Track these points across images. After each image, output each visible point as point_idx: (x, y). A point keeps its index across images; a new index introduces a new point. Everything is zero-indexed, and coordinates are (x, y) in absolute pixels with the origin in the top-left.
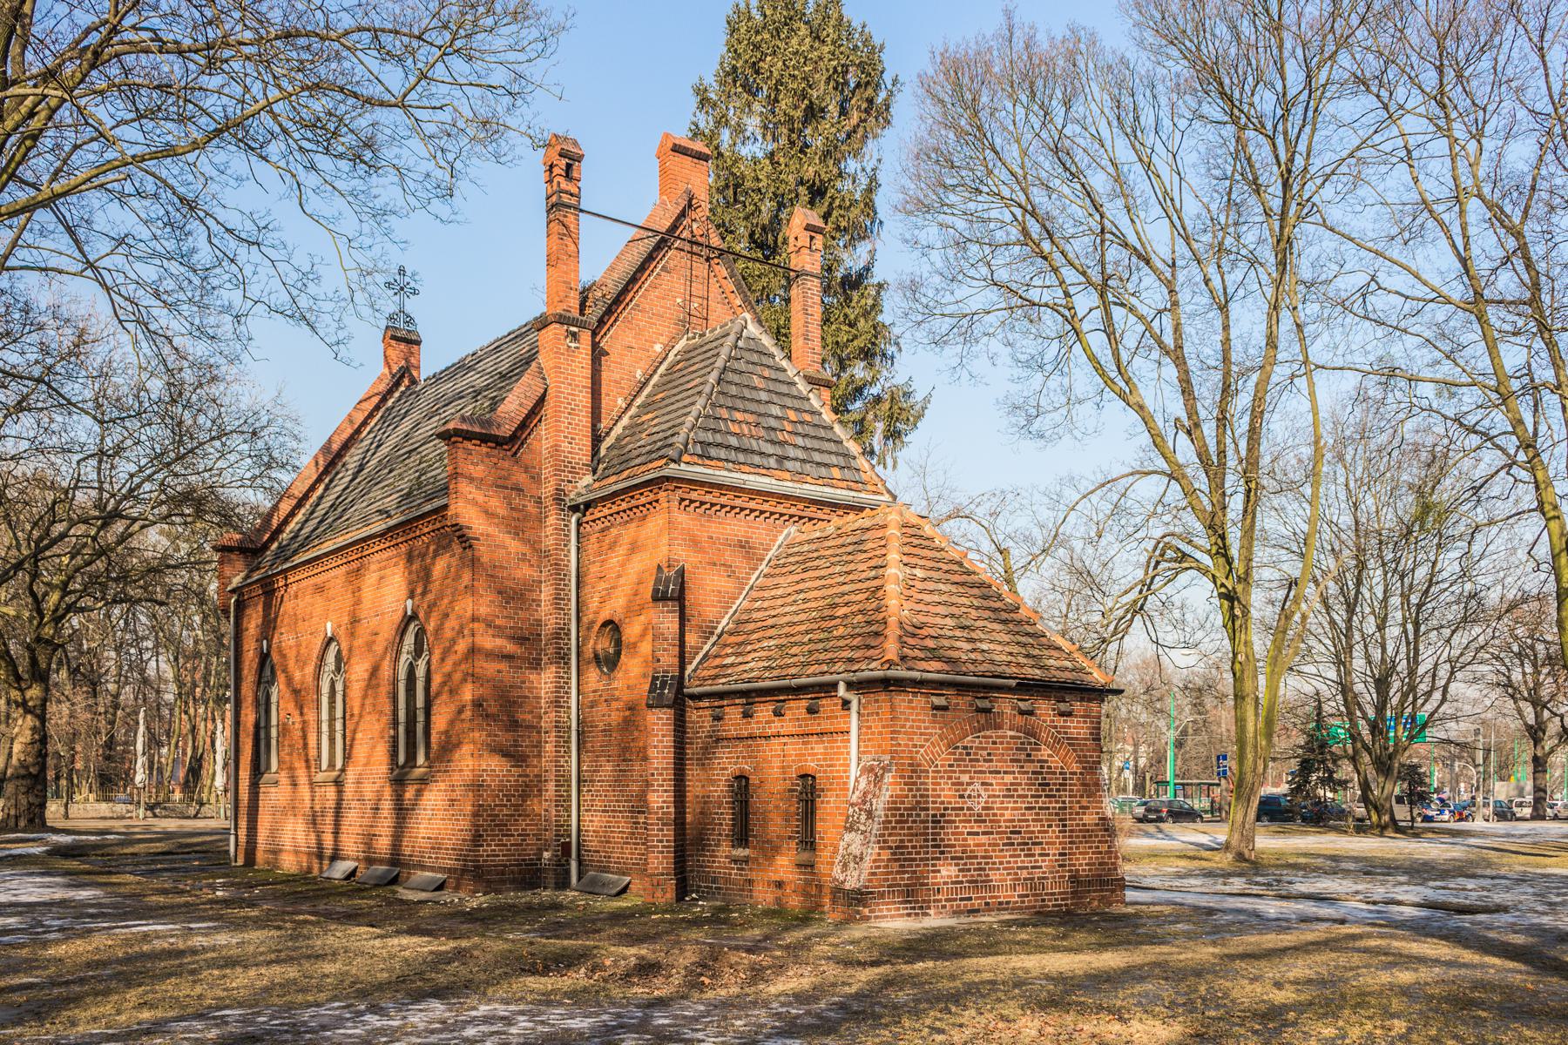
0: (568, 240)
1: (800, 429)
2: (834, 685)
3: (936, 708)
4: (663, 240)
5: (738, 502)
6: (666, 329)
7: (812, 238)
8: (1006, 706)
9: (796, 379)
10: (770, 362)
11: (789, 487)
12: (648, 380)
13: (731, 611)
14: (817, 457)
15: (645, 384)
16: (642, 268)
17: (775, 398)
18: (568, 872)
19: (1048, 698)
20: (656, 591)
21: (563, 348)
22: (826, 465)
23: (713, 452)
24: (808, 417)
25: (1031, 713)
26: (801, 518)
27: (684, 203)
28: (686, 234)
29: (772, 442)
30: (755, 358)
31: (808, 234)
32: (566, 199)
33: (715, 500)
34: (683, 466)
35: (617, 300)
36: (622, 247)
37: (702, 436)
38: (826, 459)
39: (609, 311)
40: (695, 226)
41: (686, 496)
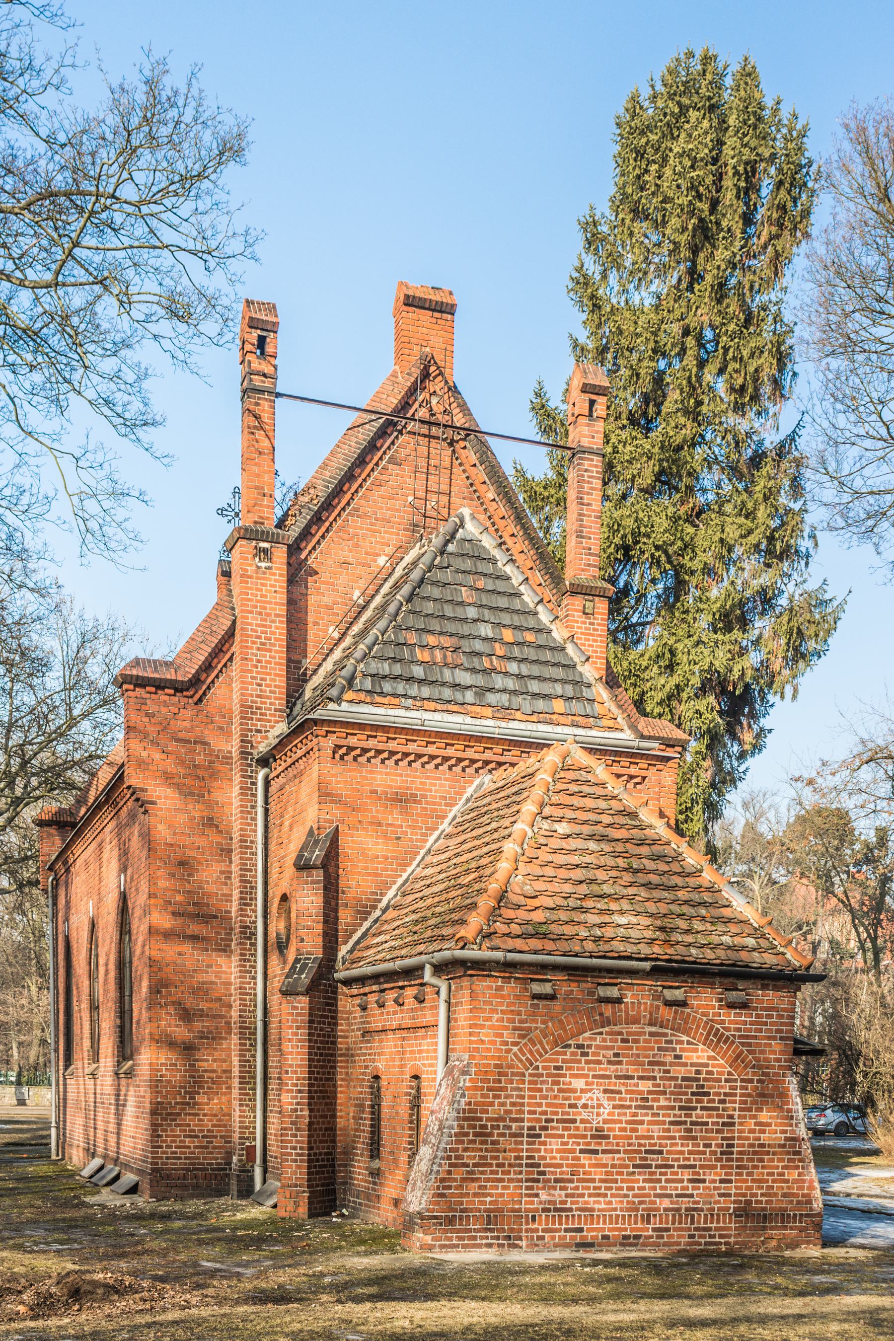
0: (260, 434)
1: (516, 652)
2: (421, 968)
3: (535, 997)
4: (390, 423)
5: (412, 747)
6: (394, 536)
7: (592, 403)
8: (637, 996)
9: (522, 588)
10: (489, 569)
11: (490, 726)
12: (368, 603)
13: (400, 881)
14: (534, 686)
15: (364, 607)
16: (361, 461)
17: (487, 614)
18: (252, 1179)
19: (712, 985)
20: (300, 857)
21: (251, 570)
22: (545, 697)
23: (387, 687)
24: (530, 637)
25: (684, 1004)
26: (500, 764)
27: (416, 372)
28: (423, 413)
29: (473, 670)
30: (468, 564)
31: (587, 397)
32: (258, 381)
33: (381, 747)
34: (345, 706)
35: (328, 505)
37: (375, 666)
38: (546, 688)
39: (317, 519)
40: (434, 400)
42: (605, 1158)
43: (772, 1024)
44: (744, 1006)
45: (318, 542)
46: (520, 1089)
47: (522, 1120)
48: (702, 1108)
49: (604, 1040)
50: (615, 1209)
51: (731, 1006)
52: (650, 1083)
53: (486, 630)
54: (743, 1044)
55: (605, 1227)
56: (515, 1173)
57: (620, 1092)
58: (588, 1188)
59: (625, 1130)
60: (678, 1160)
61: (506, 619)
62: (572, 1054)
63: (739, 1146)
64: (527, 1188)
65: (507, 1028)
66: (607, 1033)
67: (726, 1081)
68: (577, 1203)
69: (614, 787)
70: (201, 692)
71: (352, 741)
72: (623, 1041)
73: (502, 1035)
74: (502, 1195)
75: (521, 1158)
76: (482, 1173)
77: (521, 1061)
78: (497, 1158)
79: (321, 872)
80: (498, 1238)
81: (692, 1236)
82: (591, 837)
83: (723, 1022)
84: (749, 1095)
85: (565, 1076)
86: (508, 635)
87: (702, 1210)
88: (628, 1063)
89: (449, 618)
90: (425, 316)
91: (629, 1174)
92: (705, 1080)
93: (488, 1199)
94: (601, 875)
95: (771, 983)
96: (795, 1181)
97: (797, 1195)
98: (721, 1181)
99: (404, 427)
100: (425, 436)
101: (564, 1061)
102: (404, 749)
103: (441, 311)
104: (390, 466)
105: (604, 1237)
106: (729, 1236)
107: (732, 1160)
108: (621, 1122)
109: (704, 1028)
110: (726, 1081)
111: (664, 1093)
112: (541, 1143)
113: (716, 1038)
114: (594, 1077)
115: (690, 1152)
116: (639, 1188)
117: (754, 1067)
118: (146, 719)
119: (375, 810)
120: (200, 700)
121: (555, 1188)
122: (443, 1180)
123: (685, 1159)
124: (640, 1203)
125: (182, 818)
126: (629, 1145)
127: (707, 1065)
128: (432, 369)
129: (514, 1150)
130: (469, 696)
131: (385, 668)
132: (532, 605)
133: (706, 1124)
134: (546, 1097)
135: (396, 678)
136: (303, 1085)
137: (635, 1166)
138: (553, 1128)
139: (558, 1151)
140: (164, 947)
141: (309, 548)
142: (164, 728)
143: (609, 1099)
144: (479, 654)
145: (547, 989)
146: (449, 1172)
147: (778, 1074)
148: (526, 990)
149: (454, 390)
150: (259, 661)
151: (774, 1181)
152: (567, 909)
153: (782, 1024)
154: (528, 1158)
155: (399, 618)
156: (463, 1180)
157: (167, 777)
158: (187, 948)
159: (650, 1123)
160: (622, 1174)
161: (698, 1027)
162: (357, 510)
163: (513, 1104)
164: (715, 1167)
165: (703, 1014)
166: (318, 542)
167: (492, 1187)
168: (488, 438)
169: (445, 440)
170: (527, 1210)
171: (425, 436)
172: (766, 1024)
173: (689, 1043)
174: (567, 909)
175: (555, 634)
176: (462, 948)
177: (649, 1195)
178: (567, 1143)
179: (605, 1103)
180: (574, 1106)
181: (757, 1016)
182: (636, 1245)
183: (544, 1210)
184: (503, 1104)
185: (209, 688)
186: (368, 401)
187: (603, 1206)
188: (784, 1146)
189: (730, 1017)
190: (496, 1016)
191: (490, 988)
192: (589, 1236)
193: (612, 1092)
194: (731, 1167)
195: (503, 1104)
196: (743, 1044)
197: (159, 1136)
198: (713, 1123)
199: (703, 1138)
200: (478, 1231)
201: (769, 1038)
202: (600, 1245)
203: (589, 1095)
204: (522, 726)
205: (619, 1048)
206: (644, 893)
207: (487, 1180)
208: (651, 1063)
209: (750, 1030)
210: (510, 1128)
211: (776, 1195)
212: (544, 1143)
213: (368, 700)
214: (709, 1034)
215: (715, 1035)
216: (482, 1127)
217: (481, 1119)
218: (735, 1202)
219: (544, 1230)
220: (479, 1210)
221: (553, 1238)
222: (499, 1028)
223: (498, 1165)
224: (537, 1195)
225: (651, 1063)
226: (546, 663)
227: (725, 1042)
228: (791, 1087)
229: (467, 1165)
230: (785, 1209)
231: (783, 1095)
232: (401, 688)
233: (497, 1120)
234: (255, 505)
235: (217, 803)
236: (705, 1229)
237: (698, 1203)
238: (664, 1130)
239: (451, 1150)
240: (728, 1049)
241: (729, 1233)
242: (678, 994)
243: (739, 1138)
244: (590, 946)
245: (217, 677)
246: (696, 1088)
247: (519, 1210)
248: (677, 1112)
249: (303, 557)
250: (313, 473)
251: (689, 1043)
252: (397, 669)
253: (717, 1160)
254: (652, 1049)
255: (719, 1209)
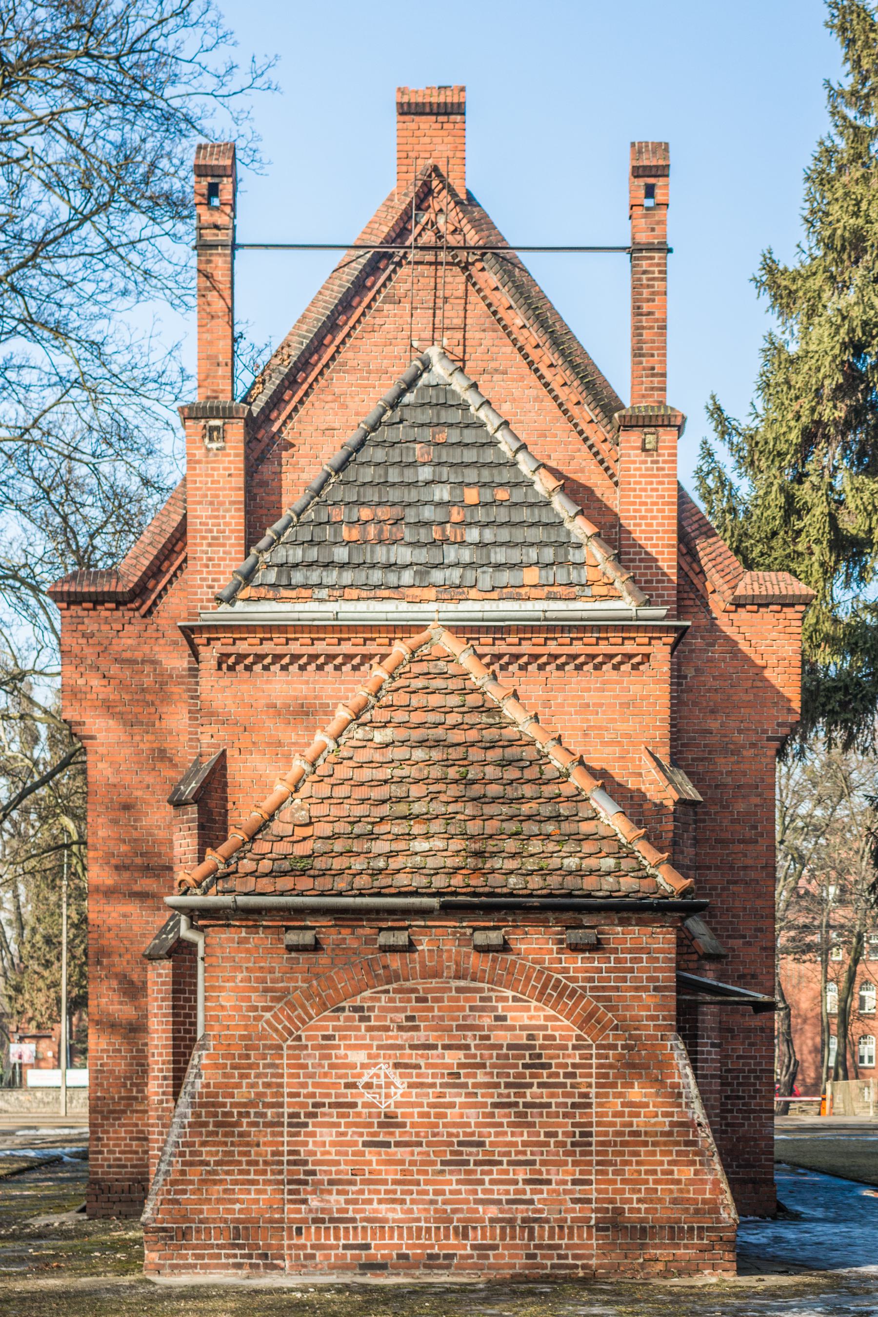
0: (212, 296)
3: (290, 948)
8: (438, 942)
9: (499, 435)
14: (499, 555)
16: (345, 305)
19: (545, 923)
23: (298, 577)
28: (429, 237)
29: (416, 544)
30: (429, 415)
32: (210, 236)
33: (279, 650)
35: (303, 363)
36: (329, 274)
38: (515, 555)
40: (441, 220)
41: (230, 649)
42: (400, 1153)
43: (640, 970)
44: (597, 947)
45: (295, 409)
46: (276, 1066)
47: (281, 1105)
48: (541, 1085)
49: (392, 1000)
50: (418, 1220)
51: (575, 948)
52: (461, 1053)
53: (442, 493)
54: (598, 999)
55: (404, 1244)
56: (273, 1173)
57: (418, 1067)
58: (378, 1192)
59: (427, 1115)
60: (508, 1154)
61: (471, 475)
62: (347, 1019)
63: (598, 1134)
64: (290, 1192)
65: (255, 990)
66: (396, 991)
67: (575, 1047)
68: (363, 1211)
69: (479, 676)
70: (149, 603)
71: (242, 647)
72: (418, 1000)
73: (249, 999)
74: (257, 1201)
75: (281, 1154)
76: (227, 1173)
77: (276, 1030)
78: (247, 1154)
79: (195, 808)
80: (250, 1256)
81: (530, 1256)
82: (421, 743)
83: (566, 970)
84: (611, 1066)
85: (338, 1047)
86: (471, 496)
87: (547, 1221)
88: (427, 1028)
89: (394, 484)
90: (426, 123)
91: (435, 1173)
92: (542, 1047)
93: (237, 1206)
94: (416, 791)
95: (634, 916)
96: (691, 1182)
97: (696, 1201)
98: (575, 1182)
99: (405, 256)
100: (430, 264)
101: (335, 1029)
102: (311, 650)
103: (446, 114)
104: (386, 307)
105: (401, 1256)
106: (590, 1257)
107: (590, 1153)
108: (421, 1105)
109: (538, 979)
110: (575, 1047)
111: (483, 1066)
112: (307, 1134)
113: (552, 990)
114: (379, 1047)
115: (525, 1144)
116: (452, 1192)
117: (616, 1028)
118: (83, 641)
119: (274, 728)
120: (150, 612)
121: (330, 1192)
122: (174, 1183)
123: (518, 1153)
124: (454, 1211)
125: (127, 751)
126: (435, 1135)
127: (545, 1028)
128: (435, 183)
129: (271, 1144)
130: (407, 577)
131: (297, 554)
132: (509, 454)
133: (549, 1105)
134: (312, 1076)
135: (310, 565)
136: (168, 1070)
137: (443, 1163)
138: (324, 1115)
139: (333, 1144)
140: (107, 908)
141: (283, 417)
142: (104, 650)
143: (401, 1076)
144: (427, 524)
145: (307, 938)
146: (183, 1173)
147: (655, 1037)
148: (280, 940)
149: (468, 203)
150: (210, 559)
151: (656, 1182)
152: (350, 836)
153: (656, 970)
154: (290, 1153)
155: (324, 493)
156: (203, 1182)
157: (108, 707)
158: (133, 908)
159: (463, 1105)
160: (426, 1173)
161: (528, 979)
162: (344, 364)
163: (267, 1085)
164: (566, 1163)
165: (535, 962)
166: (295, 409)
167: (241, 1191)
168: (521, 255)
169: (458, 264)
170: (292, 1221)
171: (430, 264)
172: (631, 970)
173: (515, 999)
174: (350, 836)
175: (538, 487)
176: (185, 893)
177: (467, 1201)
178: (344, 1134)
179: (397, 1081)
180: (354, 1085)
181: (618, 961)
182: (448, 1267)
183: (315, 1221)
184: (253, 1085)
185: (160, 596)
186: (358, 234)
187: (400, 1216)
188: (670, 1134)
189: (577, 963)
190: (240, 976)
191: (232, 940)
192: (377, 1254)
193: (406, 1066)
194: (589, 1163)
195: (253, 1085)
196: (598, 999)
197: (99, 1139)
198: (558, 1105)
199: (542, 1125)
200: (219, 1247)
201: (637, 989)
202: (394, 1267)
203: (373, 1071)
204: (477, 606)
205: (413, 1009)
206: (470, 810)
207: (235, 1182)
208: (459, 1028)
209: (609, 979)
210: (264, 1115)
211: (660, 1200)
212: (313, 1134)
213: (271, 595)
214: (545, 987)
215: (555, 988)
216: (225, 1114)
217: (224, 1105)
218: (597, 1210)
219: (313, 1247)
220: (225, 1221)
221: (327, 1257)
222: (244, 989)
223: (249, 1163)
224: (305, 1201)
225: (459, 1028)
226: (521, 524)
227: (570, 997)
228: (676, 1054)
229: (207, 1164)
230: (679, 1221)
231: (664, 1064)
232: (314, 576)
233: (244, 1105)
234: (207, 377)
235: (170, 732)
236: (550, 1247)
237: (540, 1211)
238: (485, 1115)
239: (185, 1144)
240: (576, 1005)
241: (590, 1252)
242: (495, 938)
243: (599, 1124)
244: (362, 882)
245: (170, 582)
246: (532, 1057)
247: (281, 1220)
248: (503, 1091)
249: (275, 429)
250: (290, 329)
251: (515, 999)
252: (313, 554)
253: (567, 1153)
254: (462, 1009)
255: (573, 1220)
